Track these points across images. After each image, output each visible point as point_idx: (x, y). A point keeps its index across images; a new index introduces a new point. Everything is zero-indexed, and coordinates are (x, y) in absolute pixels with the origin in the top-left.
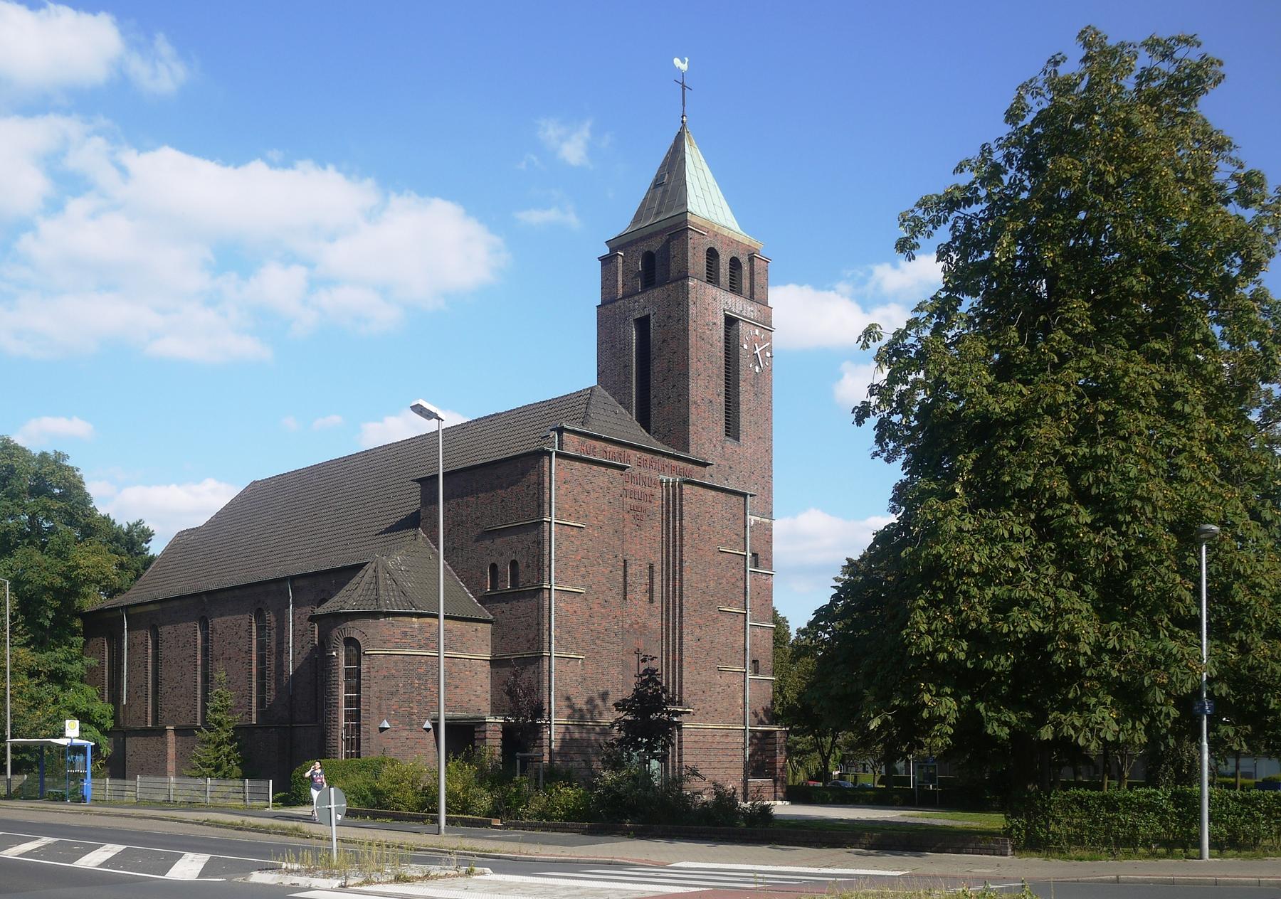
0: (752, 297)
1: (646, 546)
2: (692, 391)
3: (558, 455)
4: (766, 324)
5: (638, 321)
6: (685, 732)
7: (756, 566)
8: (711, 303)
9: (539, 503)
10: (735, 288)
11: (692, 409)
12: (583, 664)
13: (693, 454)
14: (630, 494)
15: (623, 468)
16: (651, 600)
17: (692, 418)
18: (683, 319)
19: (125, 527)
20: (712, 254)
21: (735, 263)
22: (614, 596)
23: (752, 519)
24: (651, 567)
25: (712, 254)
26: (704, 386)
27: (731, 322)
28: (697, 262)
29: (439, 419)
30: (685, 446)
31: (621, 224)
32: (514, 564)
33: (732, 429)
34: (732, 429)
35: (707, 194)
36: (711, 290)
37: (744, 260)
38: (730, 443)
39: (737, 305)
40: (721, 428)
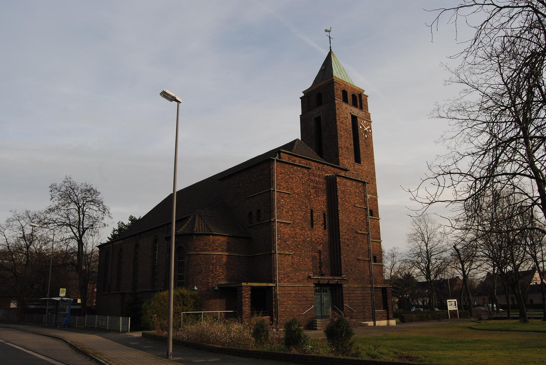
0: (361, 108)
1: (320, 204)
2: (340, 143)
3: (277, 161)
4: (368, 118)
5: (315, 119)
6: (344, 289)
7: (372, 215)
8: (345, 111)
9: (269, 183)
10: (355, 104)
11: (340, 150)
12: (292, 257)
13: (341, 166)
14: (312, 181)
15: (309, 168)
16: (325, 228)
17: (340, 153)
18: (334, 115)
19: (130, 222)
20: (345, 93)
21: (354, 96)
22: (307, 225)
23: (369, 196)
24: (324, 214)
25: (345, 93)
26: (345, 141)
27: (354, 118)
28: (338, 94)
29: (178, 101)
30: (338, 164)
31: (308, 84)
32: (259, 211)
33: (358, 160)
34: (358, 160)
35: (341, 73)
36: (344, 105)
37: (357, 96)
38: (357, 166)
39: (356, 111)
40: (352, 159)
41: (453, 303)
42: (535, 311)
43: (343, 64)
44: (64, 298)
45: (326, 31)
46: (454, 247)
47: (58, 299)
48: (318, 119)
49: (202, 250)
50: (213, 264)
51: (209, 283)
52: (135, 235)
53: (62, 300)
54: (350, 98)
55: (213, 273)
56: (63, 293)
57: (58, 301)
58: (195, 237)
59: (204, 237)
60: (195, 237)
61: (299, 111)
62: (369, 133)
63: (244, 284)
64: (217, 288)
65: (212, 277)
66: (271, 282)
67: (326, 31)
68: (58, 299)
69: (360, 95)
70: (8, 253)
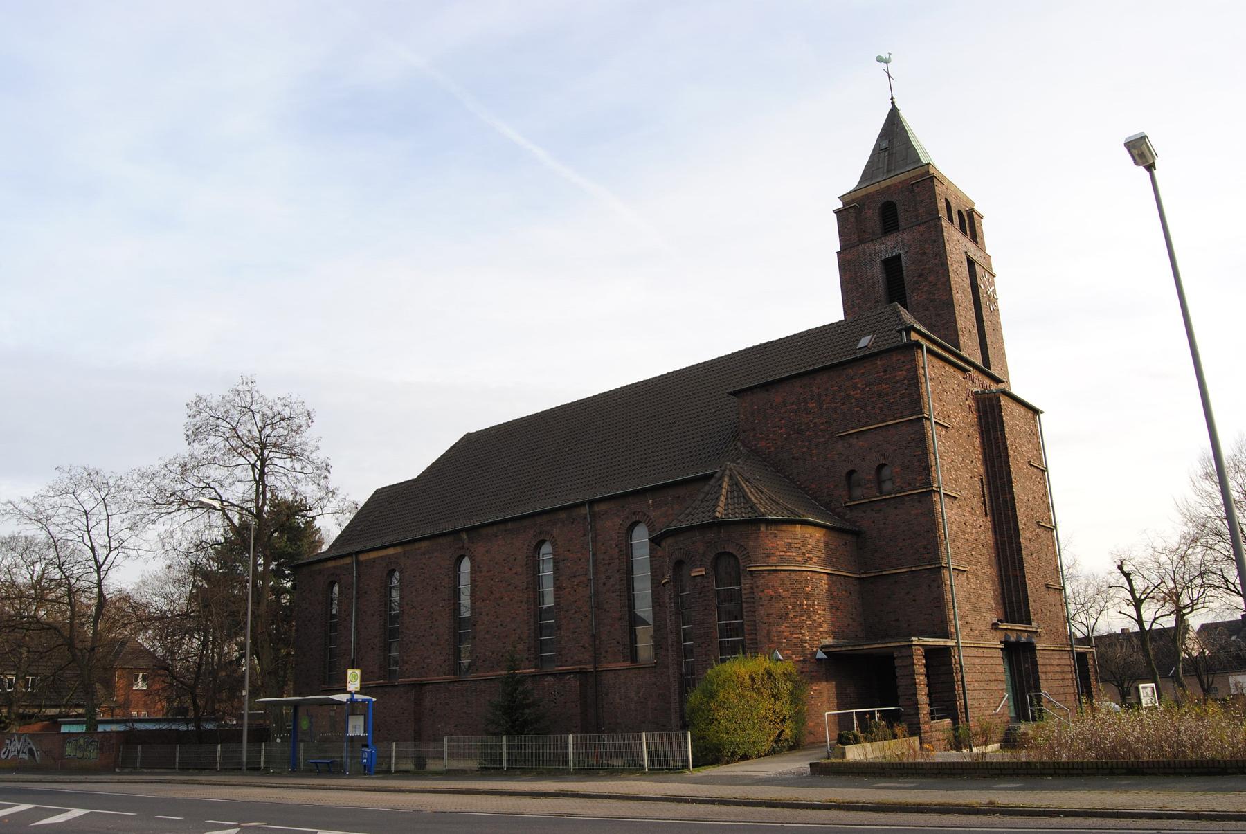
5: (886, 262)
6: (1038, 654)
31: (850, 179)
41: (1149, 690)
42: (147, 774)
43: (923, 143)
44: (357, 697)
45: (880, 60)
46: (1120, 568)
47: (343, 698)
48: (892, 266)
49: (783, 560)
50: (808, 596)
51: (805, 641)
52: (458, 532)
53: (352, 701)
54: (955, 217)
55: (809, 617)
56: (354, 680)
57: (340, 703)
58: (763, 529)
59: (784, 527)
60: (763, 529)
61: (834, 244)
62: (993, 300)
63: (915, 640)
64: (820, 655)
65: (810, 629)
66: (946, 635)
67: (880, 60)
68: (343, 698)
69: (971, 213)
70: (13, 592)
